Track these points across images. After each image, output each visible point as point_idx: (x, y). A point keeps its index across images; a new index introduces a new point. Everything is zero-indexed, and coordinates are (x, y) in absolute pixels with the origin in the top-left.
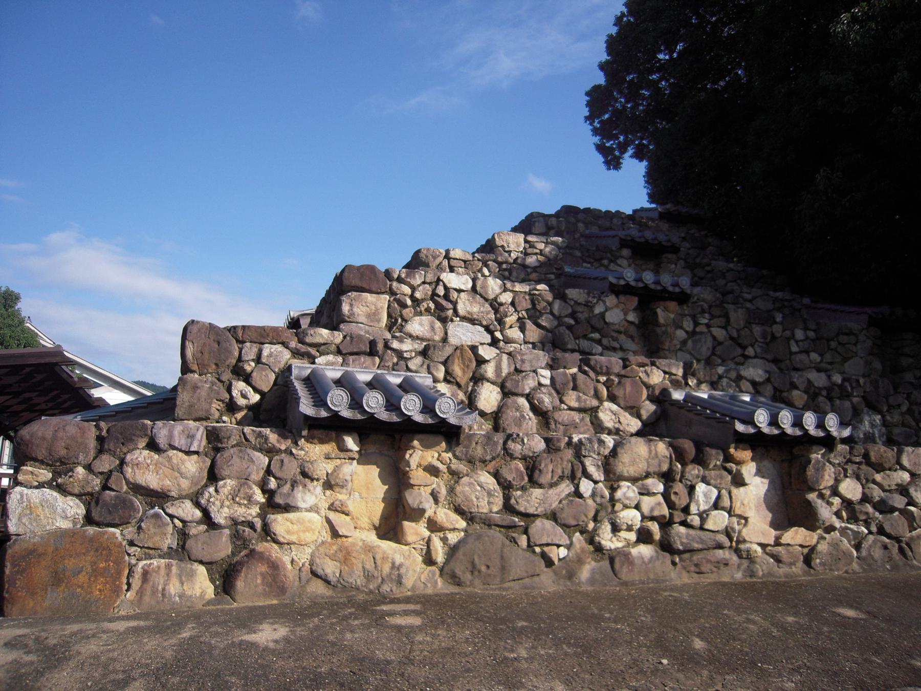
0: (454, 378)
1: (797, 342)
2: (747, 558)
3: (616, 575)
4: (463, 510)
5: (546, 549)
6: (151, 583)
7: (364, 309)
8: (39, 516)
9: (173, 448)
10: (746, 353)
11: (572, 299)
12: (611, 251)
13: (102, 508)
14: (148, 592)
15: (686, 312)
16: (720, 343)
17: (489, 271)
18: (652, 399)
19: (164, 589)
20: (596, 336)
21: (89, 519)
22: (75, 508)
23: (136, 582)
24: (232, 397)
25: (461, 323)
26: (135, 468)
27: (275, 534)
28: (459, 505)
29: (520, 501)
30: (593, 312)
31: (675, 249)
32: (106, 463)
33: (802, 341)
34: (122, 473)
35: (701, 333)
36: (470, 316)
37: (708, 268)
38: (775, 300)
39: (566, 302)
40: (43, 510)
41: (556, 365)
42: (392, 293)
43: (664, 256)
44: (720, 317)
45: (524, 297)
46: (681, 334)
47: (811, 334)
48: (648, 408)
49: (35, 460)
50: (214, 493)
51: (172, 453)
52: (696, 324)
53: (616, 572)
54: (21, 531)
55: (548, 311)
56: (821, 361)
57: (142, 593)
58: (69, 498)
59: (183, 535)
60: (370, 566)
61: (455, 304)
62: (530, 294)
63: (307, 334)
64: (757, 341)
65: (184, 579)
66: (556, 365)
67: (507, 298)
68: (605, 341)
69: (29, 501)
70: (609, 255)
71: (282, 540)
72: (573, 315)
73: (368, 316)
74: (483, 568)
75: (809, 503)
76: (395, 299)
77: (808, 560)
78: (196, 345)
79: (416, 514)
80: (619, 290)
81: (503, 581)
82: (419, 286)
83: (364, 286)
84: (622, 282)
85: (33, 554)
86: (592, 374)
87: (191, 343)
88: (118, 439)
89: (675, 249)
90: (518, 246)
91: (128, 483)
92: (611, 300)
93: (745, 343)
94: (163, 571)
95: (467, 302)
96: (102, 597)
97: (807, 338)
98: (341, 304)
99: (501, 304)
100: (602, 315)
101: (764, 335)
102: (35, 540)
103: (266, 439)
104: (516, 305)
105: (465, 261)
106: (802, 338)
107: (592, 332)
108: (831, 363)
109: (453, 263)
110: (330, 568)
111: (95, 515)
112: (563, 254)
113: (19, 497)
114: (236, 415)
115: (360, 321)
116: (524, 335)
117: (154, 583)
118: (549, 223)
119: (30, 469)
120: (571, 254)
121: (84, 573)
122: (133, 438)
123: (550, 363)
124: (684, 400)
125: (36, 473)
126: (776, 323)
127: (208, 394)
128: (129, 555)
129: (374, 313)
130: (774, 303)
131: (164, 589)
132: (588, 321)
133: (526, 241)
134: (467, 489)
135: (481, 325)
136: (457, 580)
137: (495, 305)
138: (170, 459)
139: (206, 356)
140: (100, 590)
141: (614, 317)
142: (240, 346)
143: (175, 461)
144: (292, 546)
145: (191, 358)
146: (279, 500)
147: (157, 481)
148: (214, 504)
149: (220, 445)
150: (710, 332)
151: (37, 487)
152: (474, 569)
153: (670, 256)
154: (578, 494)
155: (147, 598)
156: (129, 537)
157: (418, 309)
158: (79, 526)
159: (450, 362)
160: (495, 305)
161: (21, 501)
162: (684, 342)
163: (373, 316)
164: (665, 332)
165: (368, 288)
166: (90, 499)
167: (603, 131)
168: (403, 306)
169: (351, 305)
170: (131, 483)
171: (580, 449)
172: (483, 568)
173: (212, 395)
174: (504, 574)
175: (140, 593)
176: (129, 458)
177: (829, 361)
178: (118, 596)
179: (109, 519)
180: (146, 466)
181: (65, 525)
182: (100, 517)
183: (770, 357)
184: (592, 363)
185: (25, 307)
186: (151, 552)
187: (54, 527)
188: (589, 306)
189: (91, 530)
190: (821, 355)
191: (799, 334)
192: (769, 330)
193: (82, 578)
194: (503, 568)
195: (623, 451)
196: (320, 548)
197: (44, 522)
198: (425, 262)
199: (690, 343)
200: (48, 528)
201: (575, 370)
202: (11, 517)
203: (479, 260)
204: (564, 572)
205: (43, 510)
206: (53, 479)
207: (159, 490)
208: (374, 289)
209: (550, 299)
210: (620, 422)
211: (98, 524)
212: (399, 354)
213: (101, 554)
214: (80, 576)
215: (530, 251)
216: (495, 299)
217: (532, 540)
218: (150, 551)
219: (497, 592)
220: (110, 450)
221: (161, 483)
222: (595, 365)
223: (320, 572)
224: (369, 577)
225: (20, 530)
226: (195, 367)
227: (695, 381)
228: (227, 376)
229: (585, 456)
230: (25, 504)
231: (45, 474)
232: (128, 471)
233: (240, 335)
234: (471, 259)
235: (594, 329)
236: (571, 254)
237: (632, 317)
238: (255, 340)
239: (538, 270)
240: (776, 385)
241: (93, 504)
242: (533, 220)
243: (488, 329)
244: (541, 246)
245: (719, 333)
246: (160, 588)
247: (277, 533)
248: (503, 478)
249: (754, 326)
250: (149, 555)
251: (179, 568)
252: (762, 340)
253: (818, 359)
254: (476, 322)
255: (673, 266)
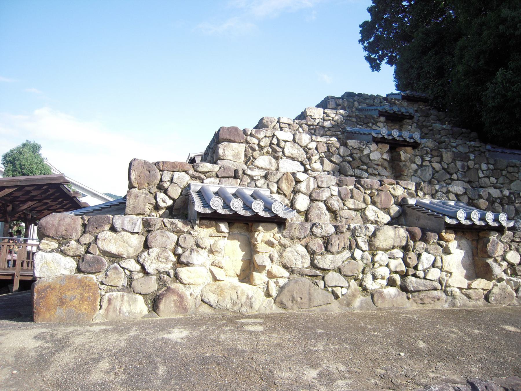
0: (282, 191)
1: (482, 171)
2: (451, 296)
3: (374, 304)
4: (287, 266)
5: (334, 289)
6: (113, 305)
7: (231, 152)
8: (51, 267)
9: (124, 230)
10: (452, 177)
11: (351, 146)
12: (373, 118)
13: (85, 263)
14: (111, 310)
15: (417, 154)
16: (437, 172)
17: (303, 130)
18: (397, 204)
19: (120, 309)
20: (365, 167)
21: (79, 270)
22: (72, 264)
23: (105, 304)
24: (157, 202)
25: (287, 160)
26: (103, 241)
27: (181, 279)
28: (285, 264)
29: (320, 261)
30: (363, 154)
31: (411, 117)
32: (87, 239)
33: (485, 170)
34: (96, 244)
35: (426, 166)
36: (292, 156)
37: (430, 128)
38: (470, 147)
39: (347, 148)
40: (54, 265)
41: (341, 184)
42: (247, 143)
43: (405, 121)
44: (437, 156)
45: (323, 145)
46: (414, 166)
47: (491, 167)
48: (394, 209)
49: (49, 236)
50: (147, 255)
51: (123, 233)
52: (423, 160)
53: (375, 303)
54: (42, 276)
55: (337, 153)
56: (497, 183)
57: (108, 310)
58: (68, 258)
59: (130, 279)
60: (234, 297)
61: (283, 149)
62: (326, 143)
63: (199, 166)
64: (459, 170)
65: (131, 303)
66: (341, 184)
67: (313, 145)
68: (370, 170)
69: (46, 259)
70: (372, 120)
71: (185, 282)
72: (351, 155)
73: (234, 156)
74: (299, 299)
75: (488, 265)
76: (249, 146)
77: (487, 298)
78: (136, 172)
79: (261, 268)
80: (378, 141)
81: (310, 306)
82: (263, 138)
83: (231, 139)
84: (380, 136)
85: (48, 288)
86: (362, 189)
87: (134, 172)
88: (94, 225)
89: (411, 117)
90: (320, 115)
91: (100, 250)
92: (373, 146)
93: (452, 171)
94: (119, 299)
95: (290, 148)
96: (87, 312)
97: (489, 169)
98: (218, 149)
99: (310, 149)
100: (368, 155)
101: (463, 167)
102: (50, 281)
103: (176, 225)
104: (319, 149)
105: (289, 125)
106: (486, 169)
107: (362, 165)
108: (502, 184)
109: (282, 125)
110: (212, 298)
111: (82, 267)
112: (345, 120)
113: (40, 257)
114: (159, 212)
115: (229, 159)
116: (323, 167)
117: (114, 305)
118: (338, 102)
119: (46, 242)
120: (350, 120)
121: (76, 299)
122: (102, 224)
123: (338, 183)
124: (415, 204)
125: (49, 244)
126: (470, 160)
127: (144, 200)
128: (101, 289)
129: (237, 154)
130: (469, 148)
131: (120, 309)
132: (360, 159)
133: (324, 113)
134: (290, 254)
135: (298, 161)
136: (284, 305)
137: (306, 150)
138: (122, 236)
139: (142, 179)
140: (85, 309)
141: (375, 156)
142: (161, 173)
143: (125, 237)
144: (191, 285)
145: (134, 180)
146: (183, 259)
147: (116, 249)
148: (147, 261)
149: (150, 229)
150: (431, 165)
151: (50, 252)
152: (293, 299)
153: (408, 121)
154: (353, 258)
155: (111, 313)
156: (101, 280)
157: (262, 152)
158: (73, 273)
159: (280, 182)
160: (306, 150)
161: (41, 259)
162: (416, 171)
163: (236, 156)
164: (405, 165)
165: (233, 140)
166: (79, 258)
167: (370, 49)
168: (254, 150)
169: (224, 150)
170: (101, 250)
171: (355, 232)
172: (299, 299)
173: (146, 201)
174: (310, 302)
175: (107, 310)
176: (100, 236)
177: (502, 182)
178: (95, 312)
179: (89, 270)
180: (109, 240)
181: (67, 273)
182: (85, 268)
183: (466, 180)
184: (362, 183)
185: (43, 153)
186: (113, 288)
187: (60, 274)
188: (360, 150)
189: (80, 276)
190: (497, 179)
191: (484, 166)
192: (466, 164)
193: (76, 302)
194: (310, 299)
195: (379, 233)
196: (206, 287)
197: (54, 271)
198: (266, 125)
199: (419, 171)
200: (56, 274)
201: (352, 187)
202: (36, 268)
203: (297, 124)
204: (345, 302)
205: (54, 265)
206: (59, 247)
207: (117, 254)
208: (237, 141)
209: (338, 146)
210: (378, 217)
211: (84, 272)
212: (251, 178)
213: (86, 289)
214: (74, 301)
215: (326, 118)
216: (306, 146)
217: (326, 283)
218: (112, 287)
219: (306, 313)
220: (89, 231)
221: (118, 250)
222: (364, 184)
223: (206, 300)
224: (234, 303)
225: (41, 275)
226: (136, 185)
227: (422, 194)
228: (154, 190)
229: (357, 236)
230: (44, 261)
231: (54, 245)
232: (99, 242)
233: (161, 167)
234: (293, 123)
235: (364, 163)
236: (350, 120)
237: (385, 156)
238: (170, 170)
239: (331, 129)
240: (470, 196)
241: (81, 261)
242: (328, 100)
243: (302, 163)
244: (333, 115)
245: (437, 166)
246: (118, 308)
247: (182, 278)
248: (310, 248)
249: (457, 162)
250: (112, 290)
251: (129, 297)
252: (462, 170)
253: (495, 181)
254: (295, 159)
255: (410, 127)
